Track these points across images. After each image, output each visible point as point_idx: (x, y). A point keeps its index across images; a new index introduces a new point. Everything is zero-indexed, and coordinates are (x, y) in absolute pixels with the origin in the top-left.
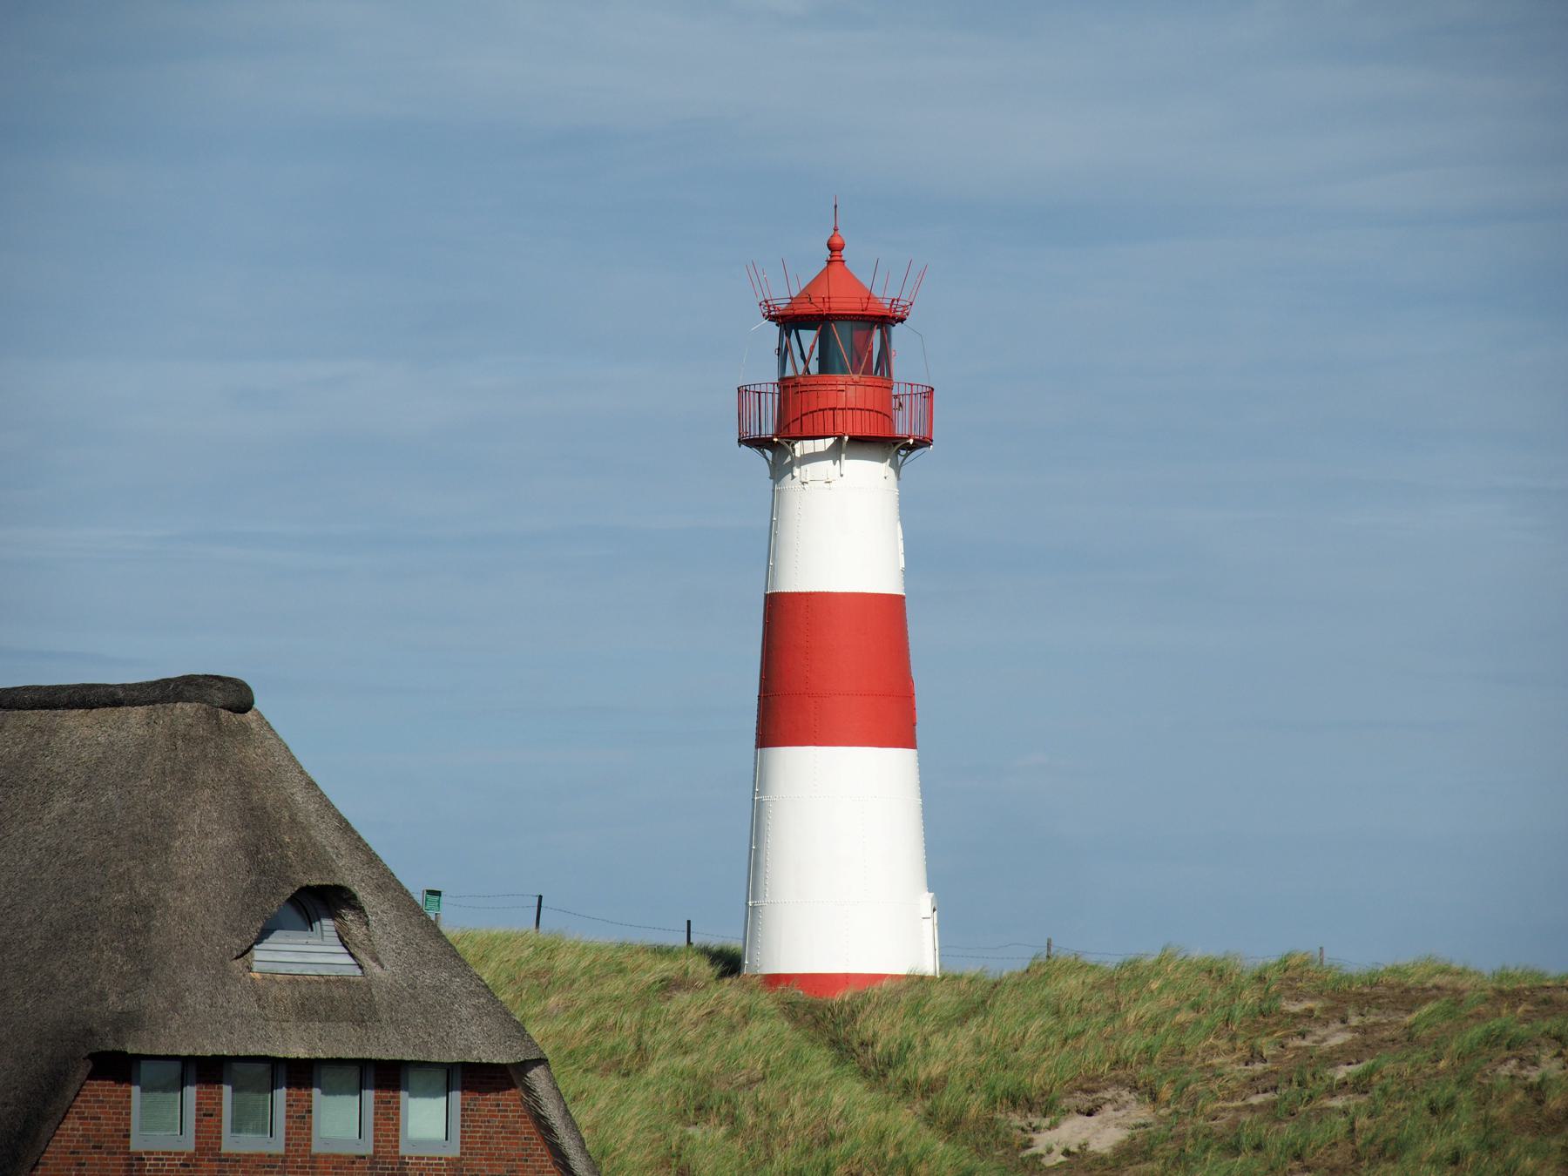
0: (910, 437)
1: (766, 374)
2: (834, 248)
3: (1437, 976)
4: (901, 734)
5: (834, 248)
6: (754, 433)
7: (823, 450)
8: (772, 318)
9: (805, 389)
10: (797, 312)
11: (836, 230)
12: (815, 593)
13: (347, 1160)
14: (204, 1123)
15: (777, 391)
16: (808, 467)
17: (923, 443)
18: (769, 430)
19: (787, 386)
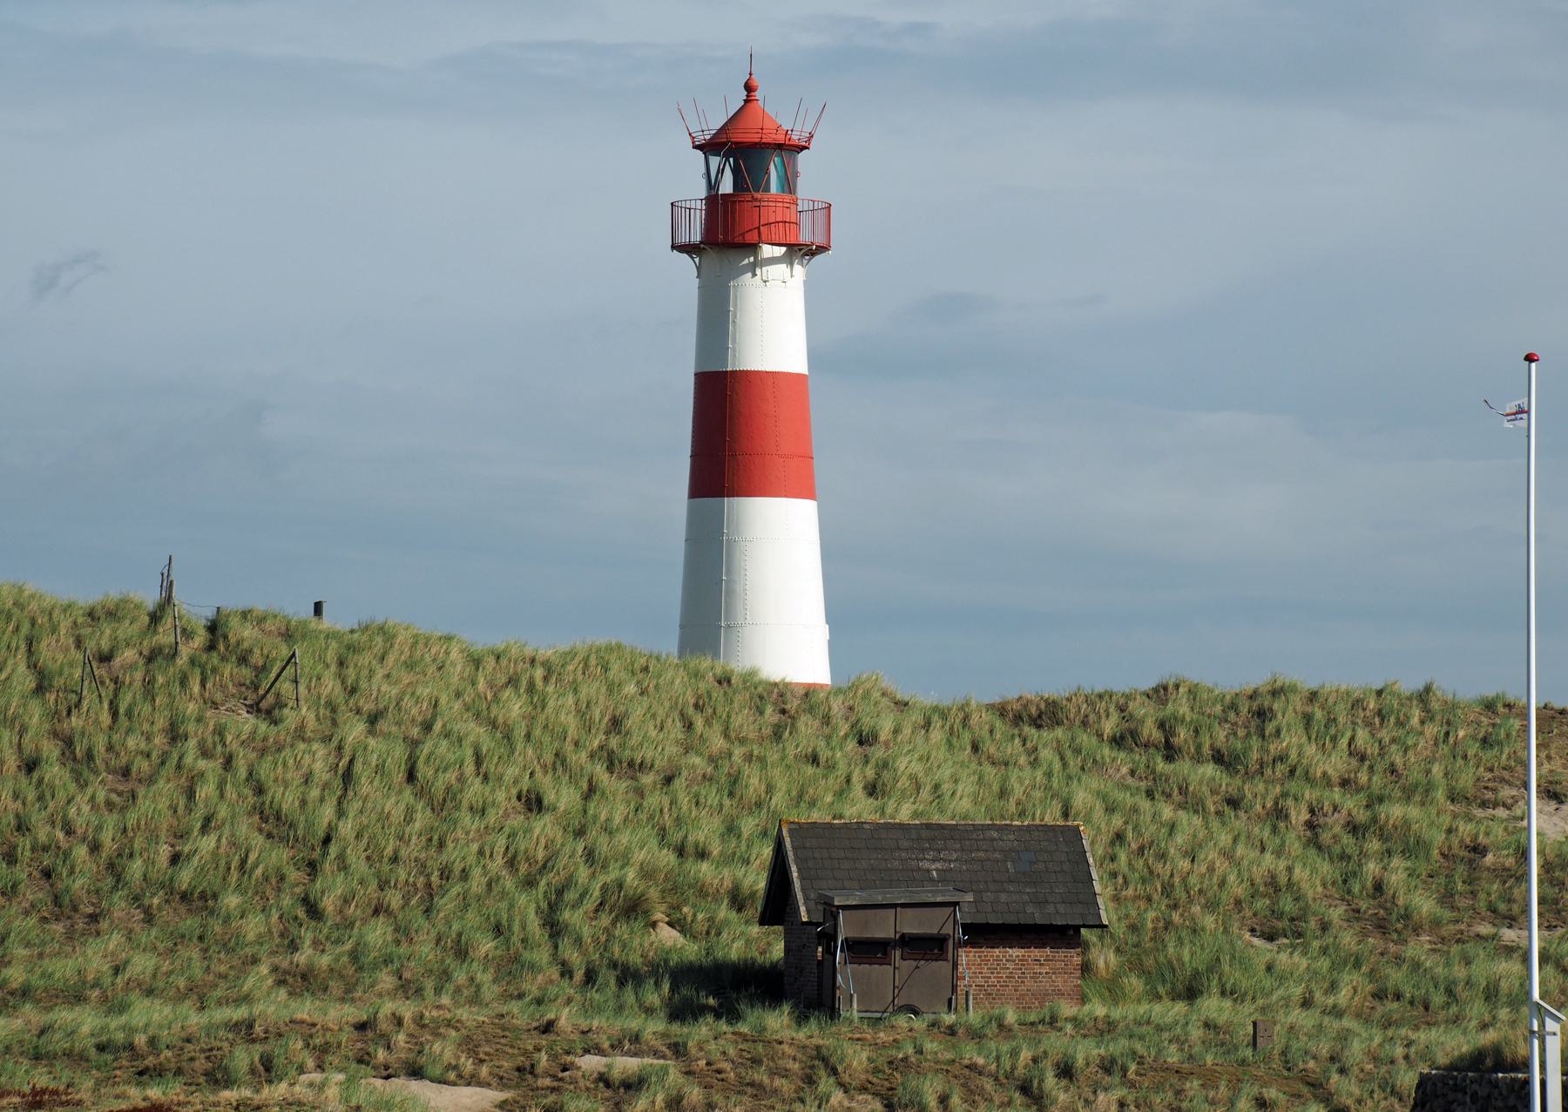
0: (813, 244)
1: (698, 190)
2: (749, 88)
3: (1325, 868)
4: (810, 495)
5: (749, 88)
6: (683, 239)
7: (779, 255)
8: (696, 147)
9: (766, 204)
10: (763, 141)
11: (751, 74)
12: (778, 373)
13: (81, 612)
14: (1103, 787)
15: (704, 207)
16: (770, 268)
17: (822, 249)
18: (697, 237)
19: (714, 201)
